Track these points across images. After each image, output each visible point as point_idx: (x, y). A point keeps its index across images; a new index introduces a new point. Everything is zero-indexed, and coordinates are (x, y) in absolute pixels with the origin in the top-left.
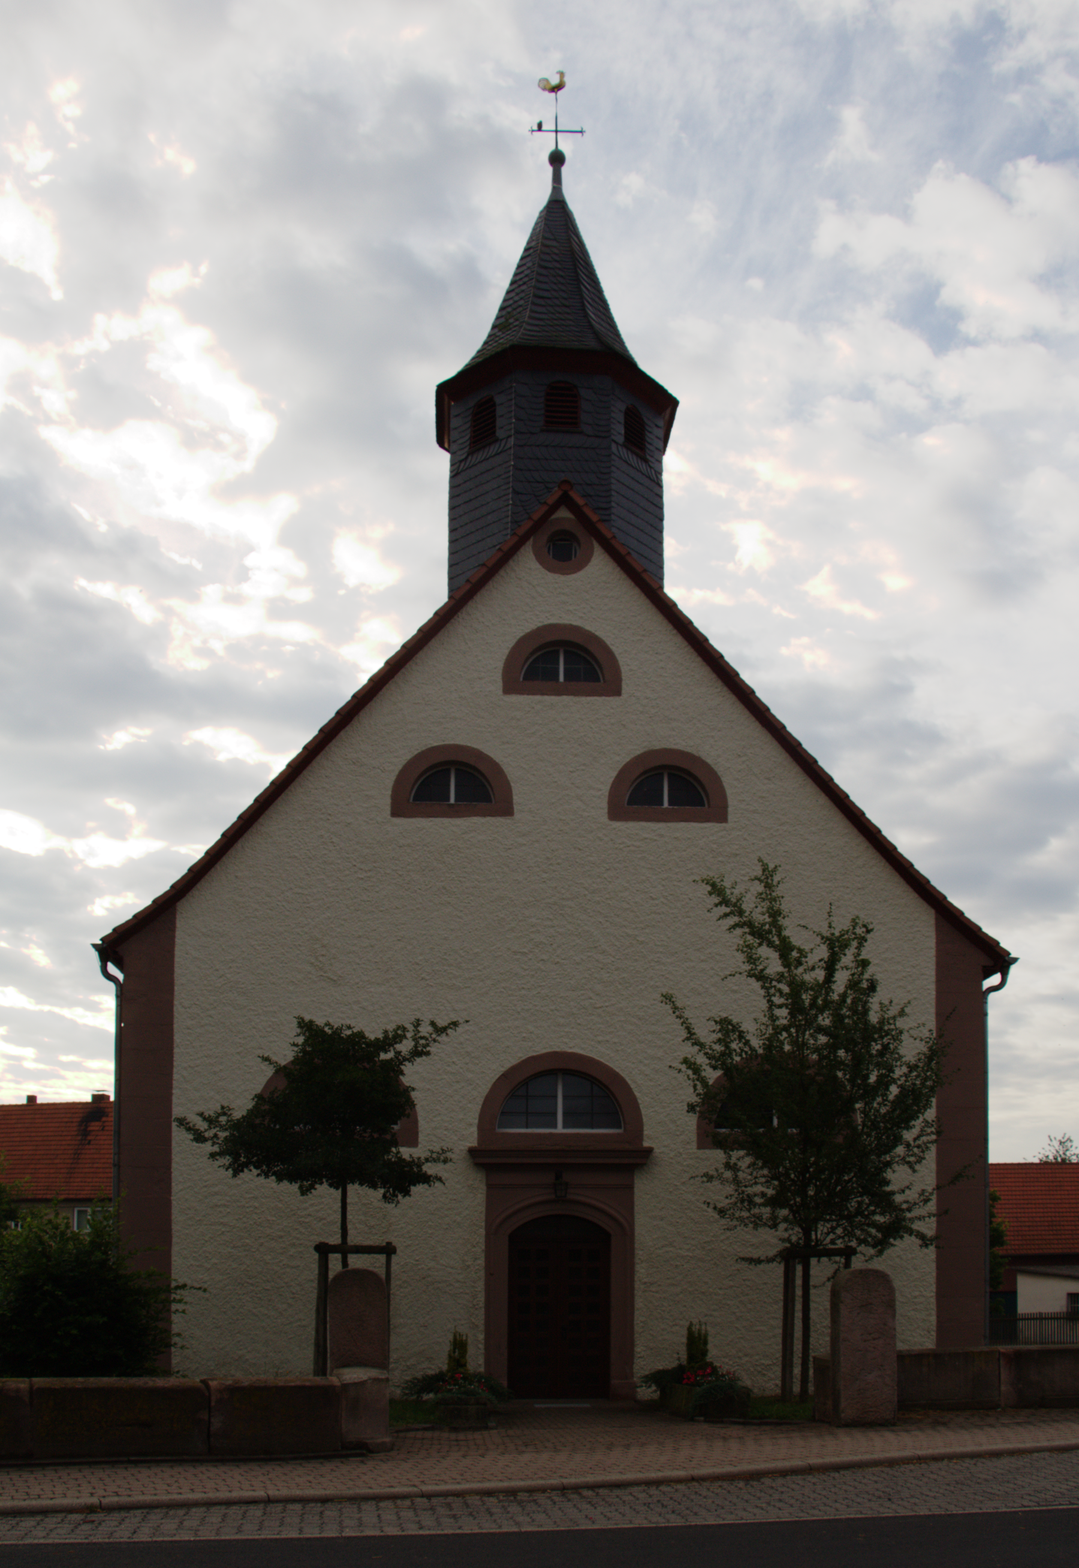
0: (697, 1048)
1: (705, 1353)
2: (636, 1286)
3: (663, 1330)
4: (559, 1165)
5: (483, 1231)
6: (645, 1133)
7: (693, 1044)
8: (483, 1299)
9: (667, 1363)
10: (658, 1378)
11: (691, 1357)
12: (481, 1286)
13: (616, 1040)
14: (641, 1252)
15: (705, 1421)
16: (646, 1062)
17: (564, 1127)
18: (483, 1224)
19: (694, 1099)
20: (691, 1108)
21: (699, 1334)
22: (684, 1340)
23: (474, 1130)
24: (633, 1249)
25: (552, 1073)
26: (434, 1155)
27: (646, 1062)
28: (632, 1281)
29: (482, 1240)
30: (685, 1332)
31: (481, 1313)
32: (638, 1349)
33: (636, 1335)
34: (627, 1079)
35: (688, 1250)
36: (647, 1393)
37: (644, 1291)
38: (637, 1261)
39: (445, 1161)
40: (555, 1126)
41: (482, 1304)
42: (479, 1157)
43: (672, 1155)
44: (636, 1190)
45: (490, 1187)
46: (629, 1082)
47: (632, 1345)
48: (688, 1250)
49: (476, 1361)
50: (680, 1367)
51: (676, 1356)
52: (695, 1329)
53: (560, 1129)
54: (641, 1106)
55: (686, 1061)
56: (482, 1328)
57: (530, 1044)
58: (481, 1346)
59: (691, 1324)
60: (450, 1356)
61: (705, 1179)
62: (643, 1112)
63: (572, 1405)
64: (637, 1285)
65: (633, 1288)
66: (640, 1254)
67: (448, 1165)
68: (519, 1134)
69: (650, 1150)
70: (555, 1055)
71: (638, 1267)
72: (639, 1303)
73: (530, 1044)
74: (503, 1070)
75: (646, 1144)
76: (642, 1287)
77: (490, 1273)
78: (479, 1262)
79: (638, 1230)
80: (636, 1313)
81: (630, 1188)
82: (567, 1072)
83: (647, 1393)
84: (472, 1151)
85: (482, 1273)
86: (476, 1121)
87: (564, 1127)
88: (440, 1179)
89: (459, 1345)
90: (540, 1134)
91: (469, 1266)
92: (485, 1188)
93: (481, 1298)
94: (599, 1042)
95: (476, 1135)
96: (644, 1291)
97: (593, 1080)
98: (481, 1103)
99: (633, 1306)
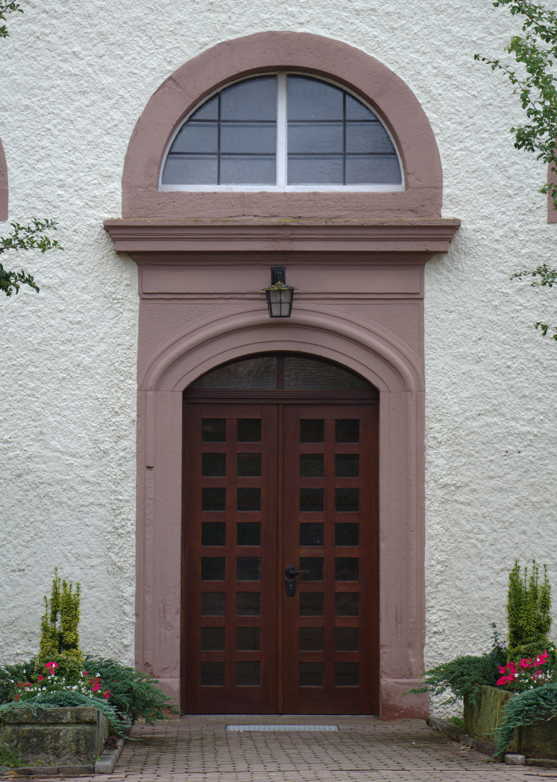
0: (521, 19)
1: (543, 627)
2: (428, 491)
3: (481, 579)
4: (278, 256)
5: (133, 385)
6: (446, 191)
7: (514, 10)
8: (133, 516)
9: (480, 648)
10: (462, 675)
11: (517, 635)
12: (129, 490)
13: (391, 9)
14: (437, 426)
15: (526, 764)
16: (449, 51)
17: (290, 181)
18: (134, 370)
19: (524, 121)
20: (524, 140)
21: (534, 588)
22: (505, 600)
23: (117, 185)
24: (421, 418)
25: (266, 74)
26: (21, 235)
27: (449, 51)
28: (421, 481)
29: (132, 401)
30: (505, 578)
31: (129, 545)
32: (431, 617)
33: (428, 590)
34: (411, 86)
35: (530, 421)
36: (446, 705)
37: (444, 502)
38: (429, 442)
39: (44, 246)
40: (273, 180)
41: (131, 527)
42: (146, 247)
43: (498, 234)
44: (427, 304)
45: (146, 297)
46: (416, 92)
47: (422, 609)
48: (530, 421)
49: (110, 632)
50: (499, 653)
51: (491, 631)
52: (524, 578)
53: (282, 185)
54: (438, 140)
55: (516, 45)
56: (131, 572)
57: (223, 17)
58: (130, 609)
59: (517, 569)
60: (45, 629)
61: (539, 279)
62: (441, 152)
63: (302, 728)
64: (430, 489)
65: (421, 496)
66: (434, 428)
67: (51, 255)
68: (203, 195)
69: (453, 227)
70: (270, 38)
71: (430, 455)
72: (433, 524)
73: (223, 17)
74: (172, 68)
75: (448, 213)
76: (441, 493)
77: (146, 467)
78: (125, 443)
79: (432, 381)
80: (429, 544)
81: (416, 298)
82: (296, 73)
83: (446, 705)
84: (110, 228)
85: (132, 465)
86: (120, 170)
87: (290, 181)
88: (29, 281)
89: (64, 606)
90: (242, 196)
91: (105, 452)
92: (137, 300)
93: (130, 513)
94: (358, 12)
95: (119, 197)
96: (444, 502)
97: (347, 90)
98: (129, 134)
99: (422, 531)
